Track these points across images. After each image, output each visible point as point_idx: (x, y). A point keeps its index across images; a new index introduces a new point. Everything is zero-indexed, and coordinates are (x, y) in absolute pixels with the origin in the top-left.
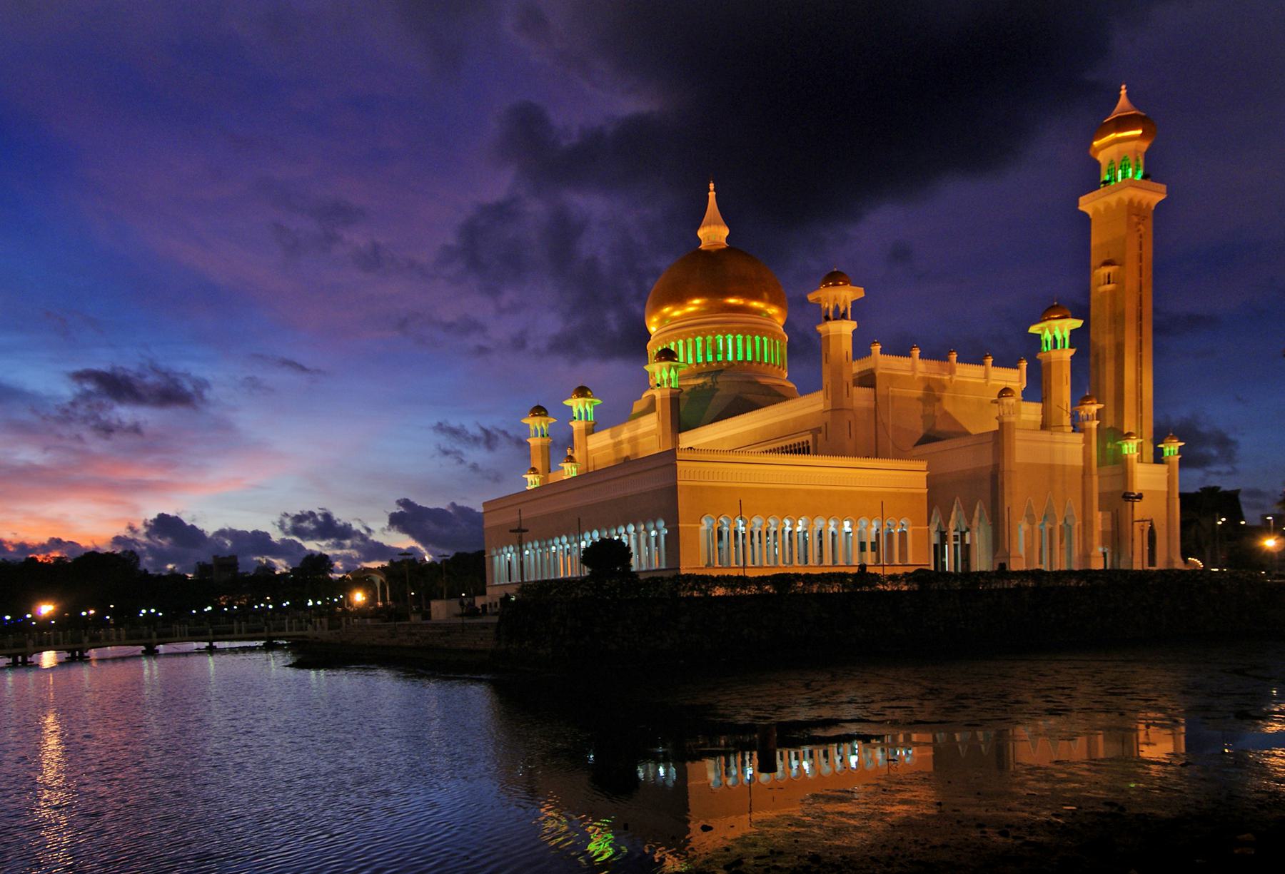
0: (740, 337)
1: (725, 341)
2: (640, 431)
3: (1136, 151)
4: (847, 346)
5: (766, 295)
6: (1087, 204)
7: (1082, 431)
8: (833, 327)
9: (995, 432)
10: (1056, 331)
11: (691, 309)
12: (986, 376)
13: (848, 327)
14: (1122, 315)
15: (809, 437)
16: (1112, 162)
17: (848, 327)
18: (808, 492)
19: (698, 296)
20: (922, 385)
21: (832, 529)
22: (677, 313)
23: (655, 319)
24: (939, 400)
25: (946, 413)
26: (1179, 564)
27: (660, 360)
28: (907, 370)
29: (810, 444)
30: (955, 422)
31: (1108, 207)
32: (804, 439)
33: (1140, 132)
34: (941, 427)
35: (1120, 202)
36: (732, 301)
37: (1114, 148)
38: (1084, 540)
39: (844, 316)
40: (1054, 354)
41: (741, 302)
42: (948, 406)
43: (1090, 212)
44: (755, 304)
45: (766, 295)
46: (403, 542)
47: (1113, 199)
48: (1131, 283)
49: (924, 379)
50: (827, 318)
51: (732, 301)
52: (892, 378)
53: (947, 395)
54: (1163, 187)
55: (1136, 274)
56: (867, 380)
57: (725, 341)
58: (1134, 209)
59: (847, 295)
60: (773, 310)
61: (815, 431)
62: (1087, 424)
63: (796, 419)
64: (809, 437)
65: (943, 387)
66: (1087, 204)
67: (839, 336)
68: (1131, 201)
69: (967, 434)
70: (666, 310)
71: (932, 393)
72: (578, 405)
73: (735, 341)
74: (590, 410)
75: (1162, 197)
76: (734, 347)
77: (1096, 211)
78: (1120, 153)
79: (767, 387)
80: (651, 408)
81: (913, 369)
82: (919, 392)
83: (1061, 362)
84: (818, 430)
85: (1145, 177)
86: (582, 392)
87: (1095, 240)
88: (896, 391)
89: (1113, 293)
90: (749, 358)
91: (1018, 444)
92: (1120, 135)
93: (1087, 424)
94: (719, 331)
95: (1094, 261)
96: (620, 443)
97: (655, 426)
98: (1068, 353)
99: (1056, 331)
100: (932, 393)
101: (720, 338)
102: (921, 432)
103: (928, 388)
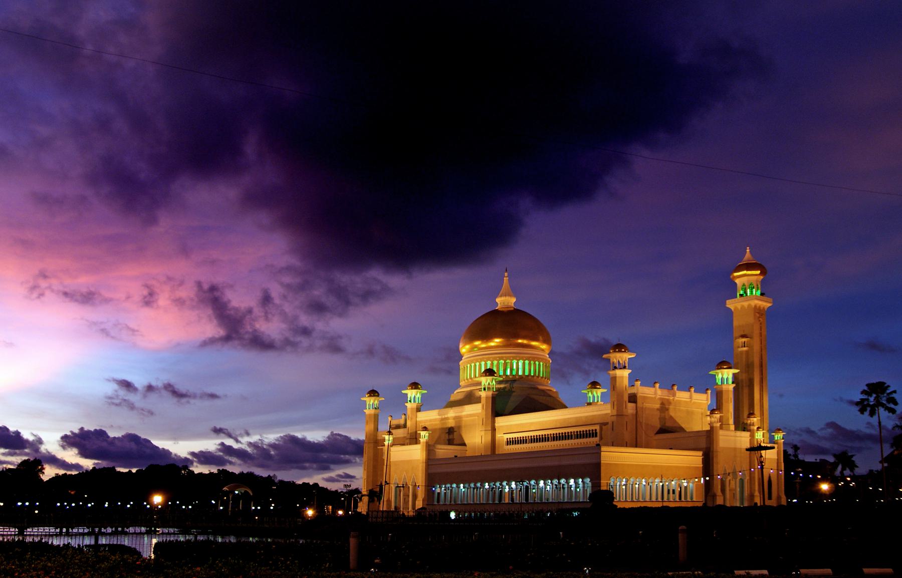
0: (527, 362)
1: (517, 364)
2: (464, 413)
3: (757, 281)
4: (626, 382)
5: (541, 338)
6: (731, 304)
7: (749, 431)
8: (618, 372)
9: (707, 431)
10: (725, 376)
11: (492, 344)
12: (691, 397)
13: (626, 373)
14: (752, 363)
15: (597, 427)
16: (744, 285)
17: (626, 373)
18: (654, 467)
19: (497, 337)
20: (659, 402)
21: (685, 484)
22: (483, 346)
23: (468, 347)
24: (668, 409)
25: (671, 417)
26: (784, 502)
27: (486, 376)
28: (651, 394)
29: (598, 431)
30: (675, 421)
31: (742, 307)
32: (594, 428)
33: (758, 272)
34: (669, 424)
35: (749, 305)
36: (520, 341)
37: (745, 278)
38: (751, 488)
39: (625, 367)
40: (724, 387)
41: (525, 342)
42: (672, 413)
43: (732, 309)
44: (534, 343)
45: (541, 338)
46: (71, 456)
47: (746, 304)
48: (757, 347)
49: (661, 399)
50: (615, 368)
51: (520, 341)
52: (645, 398)
53: (671, 407)
54: (771, 300)
55: (759, 342)
56: (633, 398)
57: (517, 364)
58: (758, 311)
59: (625, 357)
60: (544, 347)
61: (603, 425)
62: (752, 427)
63: (586, 417)
64: (597, 427)
65: (669, 403)
66: (731, 304)
67: (622, 377)
68: (755, 306)
69: (681, 430)
70: (477, 343)
71: (664, 406)
72: (411, 393)
73: (524, 364)
74: (419, 396)
75: (769, 305)
76: (521, 367)
77: (736, 308)
78: (748, 281)
79: (543, 391)
80: (470, 399)
81: (655, 393)
82: (658, 406)
83: (728, 391)
84: (606, 424)
85: (762, 294)
86: (415, 386)
87: (736, 323)
88: (647, 405)
89: (747, 352)
90: (527, 373)
91: (721, 437)
92: (749, 272)
93: (752, 427)
94: (514, 358)
95: (736, 334)
96: (447, 419)
97: (480, 411)
98: (731, 387)
99: (725, 376)
100: (664, 406)
101: (515, 362)
102: (659, 426)
103: (662, 404)
